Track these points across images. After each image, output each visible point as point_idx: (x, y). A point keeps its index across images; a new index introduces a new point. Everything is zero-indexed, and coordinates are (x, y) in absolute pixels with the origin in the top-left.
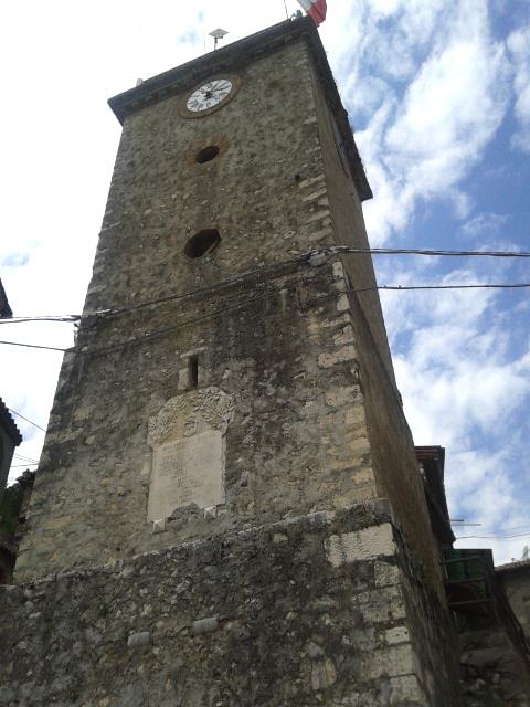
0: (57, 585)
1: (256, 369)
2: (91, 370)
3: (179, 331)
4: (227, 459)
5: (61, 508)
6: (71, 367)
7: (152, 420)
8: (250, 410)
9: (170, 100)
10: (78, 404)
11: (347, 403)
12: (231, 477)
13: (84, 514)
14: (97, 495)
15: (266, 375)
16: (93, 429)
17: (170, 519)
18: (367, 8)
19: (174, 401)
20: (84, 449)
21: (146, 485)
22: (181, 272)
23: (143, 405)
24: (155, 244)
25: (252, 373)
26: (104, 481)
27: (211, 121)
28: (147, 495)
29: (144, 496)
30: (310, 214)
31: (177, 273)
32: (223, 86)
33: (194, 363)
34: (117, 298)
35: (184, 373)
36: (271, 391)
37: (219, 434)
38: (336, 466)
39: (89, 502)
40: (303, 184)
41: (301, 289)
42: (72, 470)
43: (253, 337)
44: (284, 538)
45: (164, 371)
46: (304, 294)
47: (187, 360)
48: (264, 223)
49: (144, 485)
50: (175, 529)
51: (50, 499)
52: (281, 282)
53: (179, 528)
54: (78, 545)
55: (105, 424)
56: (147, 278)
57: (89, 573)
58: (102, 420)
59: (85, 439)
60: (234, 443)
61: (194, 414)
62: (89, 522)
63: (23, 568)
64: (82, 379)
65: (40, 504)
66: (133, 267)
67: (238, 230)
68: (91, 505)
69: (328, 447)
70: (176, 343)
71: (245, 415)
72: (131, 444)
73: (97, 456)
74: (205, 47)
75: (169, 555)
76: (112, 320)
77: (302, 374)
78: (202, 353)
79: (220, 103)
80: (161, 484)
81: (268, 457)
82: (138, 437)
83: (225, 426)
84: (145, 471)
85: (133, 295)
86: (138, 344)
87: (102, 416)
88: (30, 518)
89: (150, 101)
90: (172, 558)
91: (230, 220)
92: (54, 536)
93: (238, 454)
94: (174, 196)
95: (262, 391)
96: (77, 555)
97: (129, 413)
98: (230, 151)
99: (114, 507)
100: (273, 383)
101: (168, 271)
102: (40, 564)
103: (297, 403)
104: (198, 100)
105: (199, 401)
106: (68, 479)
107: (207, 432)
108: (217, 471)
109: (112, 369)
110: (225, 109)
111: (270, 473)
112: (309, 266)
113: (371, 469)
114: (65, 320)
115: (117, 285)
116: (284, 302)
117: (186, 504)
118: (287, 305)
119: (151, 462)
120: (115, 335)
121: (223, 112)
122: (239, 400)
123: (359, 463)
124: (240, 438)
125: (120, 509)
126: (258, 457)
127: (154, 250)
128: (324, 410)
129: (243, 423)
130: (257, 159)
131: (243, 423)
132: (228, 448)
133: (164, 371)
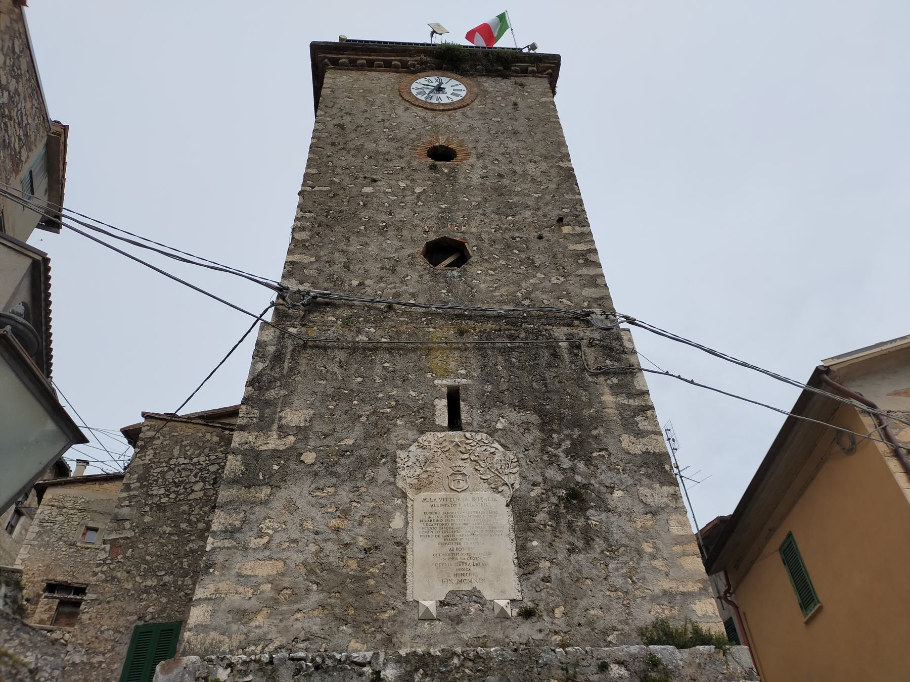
0: (274, 671)
1: (542, 427)
2: (303, 361)
3: (430, 349)
4: (517, 537)
5: (266, 546)
6: (271, 349)
7: (401, 454)
8: (540, 479)
9: (387, 75)
10: (286, 402)
11: (667, 506)
12: (526, 564)
13: (305, 564)
14: (326, 541)
15: (556, 440)
16: (312, 443)
17: (442, 604)
18: (807, 623)
19: (429, 436)
20: (300, 467)
21: (402, 544)
22: (421, 277)
23: (388, 432)
24: (383, 231)
25: (536, 433)
26: (333, 522)
27: (442, 119)
28: (404, 558)
29: (399, 560)
30: (579, 267)
31: (416, 276)
32: (454, 89)
33: (454, 397)
34: (330, 278)
35: (442, 405)
36: (566, 463)
37: (502, 500)
38: (666, 585)
39: (313, 548)
40: (566, 230)
41: (587, 349)
42: (283, 494)
43: (532, 387)
44: (623, 672)
45: (413, 394)
46: (590, 356)
47: (445, 390)
48: (523, 256)
49: (398, 544)
50: (451, 619)
51: (246, 528)
52: (560, 332)
53: (457, 620)
54: (299, 611)
55: (330, 441)
56: (374, 269)
57: (329, 662)
58: (326, 436)
59: (300, 454)
60: (523, 516)
61: (460, 463)
62: (313, 578)
63: (202, 628)
64: (291, 369)
65: (230, 532)
66: (351, 249)
67: (491, 253)
68: (316, 554)
69: (653, 557)
70: (424, 362)
71: (535, 484)
72: (373, 480)
73: (321, 483)
74: (422, 37)
75: (456, 661)
76: (327, 304)
77: (602, 453)
78: (466, 387)
79: (453, 103)
80: (422, 549)
81: (572, 550)
82: (383, 473)
83: (508, 492)
84: (397, 522)
85: (355, 283)
86: (374, 348)
87: (326, 429)
88: (214, 549)
89: (362, 65)
90: (462, 665)
91: (479, 238)
92: (256, 587)
93: (530, 534)
94: (402, 185)
95: (553, 460)
96: (298, 625)
97: (367, 437)
98: (472, 160)
99: (353, 564)
100: (567, 452)
101: (402, 270)
102: (234, 627)
103: (604, 490)
104: (420, 86)
105: (468, 447)
106: (277, 505)
107: (485, 493)
108: (505, 551)
109: (336, 370)
110: (459, 112)
111: (580, 572)
112: (589, 324)
113: (713, 601)
114: (267, 285)
115: (331, 263)
116: (566, 356)
117: (466, 587)
118: (571, 362)
119: (405, 510)
120: (330, 326)
121: (458, 114)
122: (523, 462)
123: (696, 589)
124: (532, 514)
125: (364, 570)
126: (561, 546)
127: (381, 238)
128: (638, 508)
129: (533, 494)
130: (506, 181)
131: (533, 494)
132: (516, 522)
133: (413, 394)
